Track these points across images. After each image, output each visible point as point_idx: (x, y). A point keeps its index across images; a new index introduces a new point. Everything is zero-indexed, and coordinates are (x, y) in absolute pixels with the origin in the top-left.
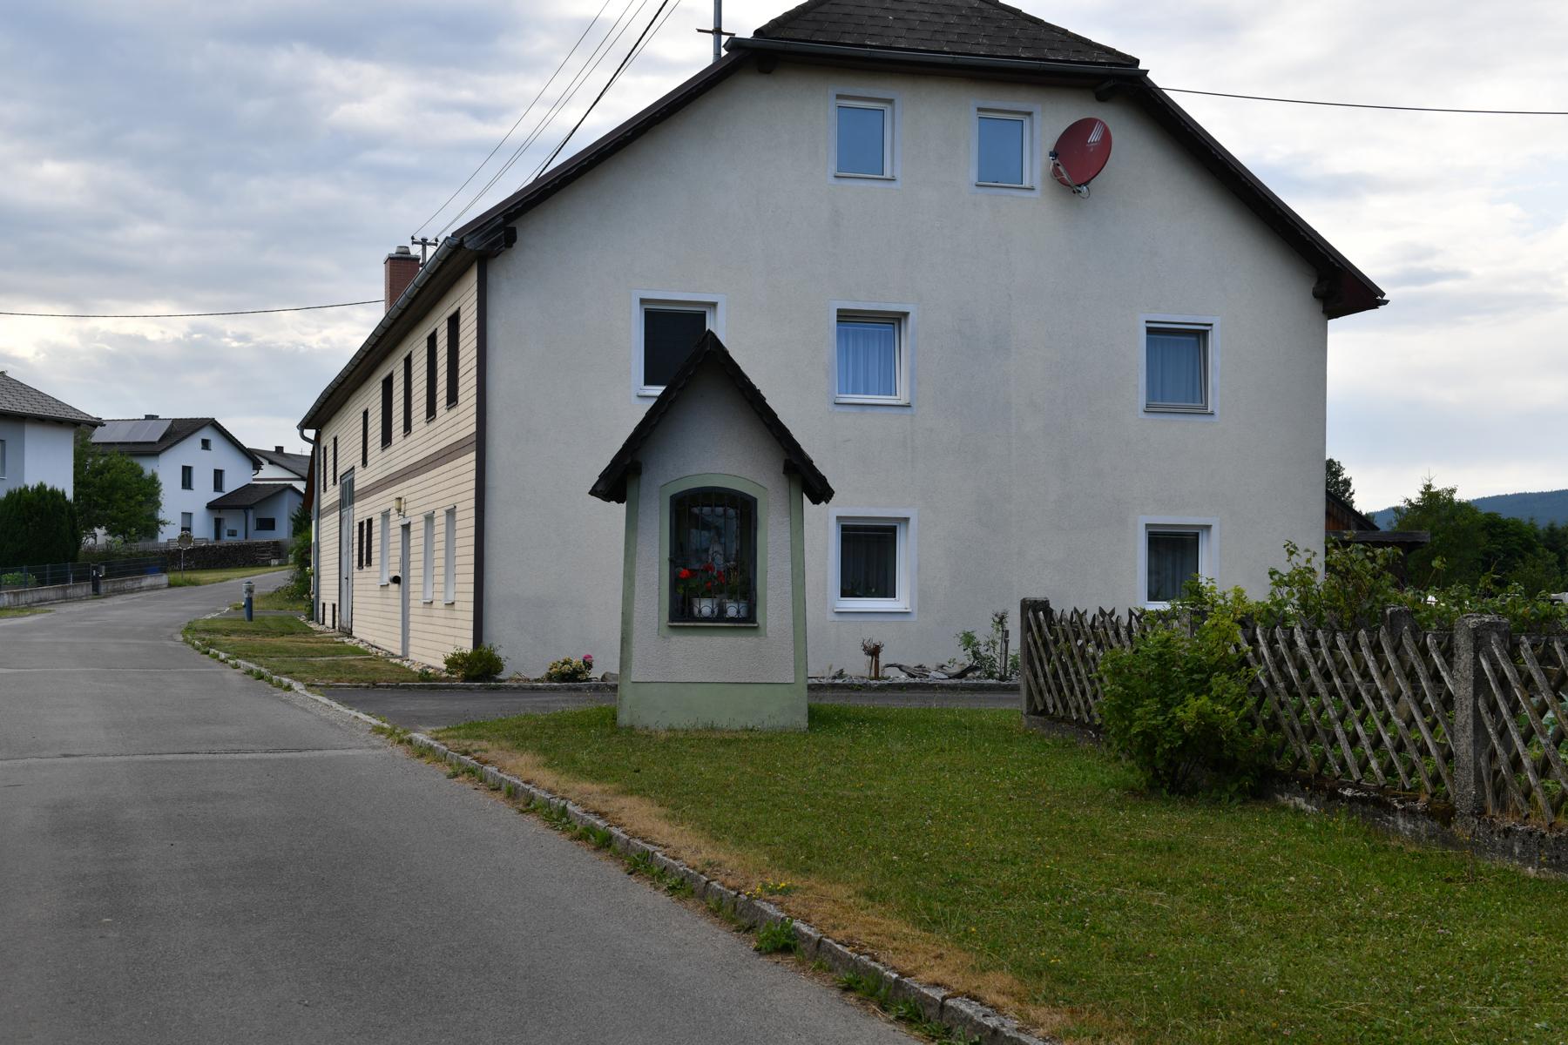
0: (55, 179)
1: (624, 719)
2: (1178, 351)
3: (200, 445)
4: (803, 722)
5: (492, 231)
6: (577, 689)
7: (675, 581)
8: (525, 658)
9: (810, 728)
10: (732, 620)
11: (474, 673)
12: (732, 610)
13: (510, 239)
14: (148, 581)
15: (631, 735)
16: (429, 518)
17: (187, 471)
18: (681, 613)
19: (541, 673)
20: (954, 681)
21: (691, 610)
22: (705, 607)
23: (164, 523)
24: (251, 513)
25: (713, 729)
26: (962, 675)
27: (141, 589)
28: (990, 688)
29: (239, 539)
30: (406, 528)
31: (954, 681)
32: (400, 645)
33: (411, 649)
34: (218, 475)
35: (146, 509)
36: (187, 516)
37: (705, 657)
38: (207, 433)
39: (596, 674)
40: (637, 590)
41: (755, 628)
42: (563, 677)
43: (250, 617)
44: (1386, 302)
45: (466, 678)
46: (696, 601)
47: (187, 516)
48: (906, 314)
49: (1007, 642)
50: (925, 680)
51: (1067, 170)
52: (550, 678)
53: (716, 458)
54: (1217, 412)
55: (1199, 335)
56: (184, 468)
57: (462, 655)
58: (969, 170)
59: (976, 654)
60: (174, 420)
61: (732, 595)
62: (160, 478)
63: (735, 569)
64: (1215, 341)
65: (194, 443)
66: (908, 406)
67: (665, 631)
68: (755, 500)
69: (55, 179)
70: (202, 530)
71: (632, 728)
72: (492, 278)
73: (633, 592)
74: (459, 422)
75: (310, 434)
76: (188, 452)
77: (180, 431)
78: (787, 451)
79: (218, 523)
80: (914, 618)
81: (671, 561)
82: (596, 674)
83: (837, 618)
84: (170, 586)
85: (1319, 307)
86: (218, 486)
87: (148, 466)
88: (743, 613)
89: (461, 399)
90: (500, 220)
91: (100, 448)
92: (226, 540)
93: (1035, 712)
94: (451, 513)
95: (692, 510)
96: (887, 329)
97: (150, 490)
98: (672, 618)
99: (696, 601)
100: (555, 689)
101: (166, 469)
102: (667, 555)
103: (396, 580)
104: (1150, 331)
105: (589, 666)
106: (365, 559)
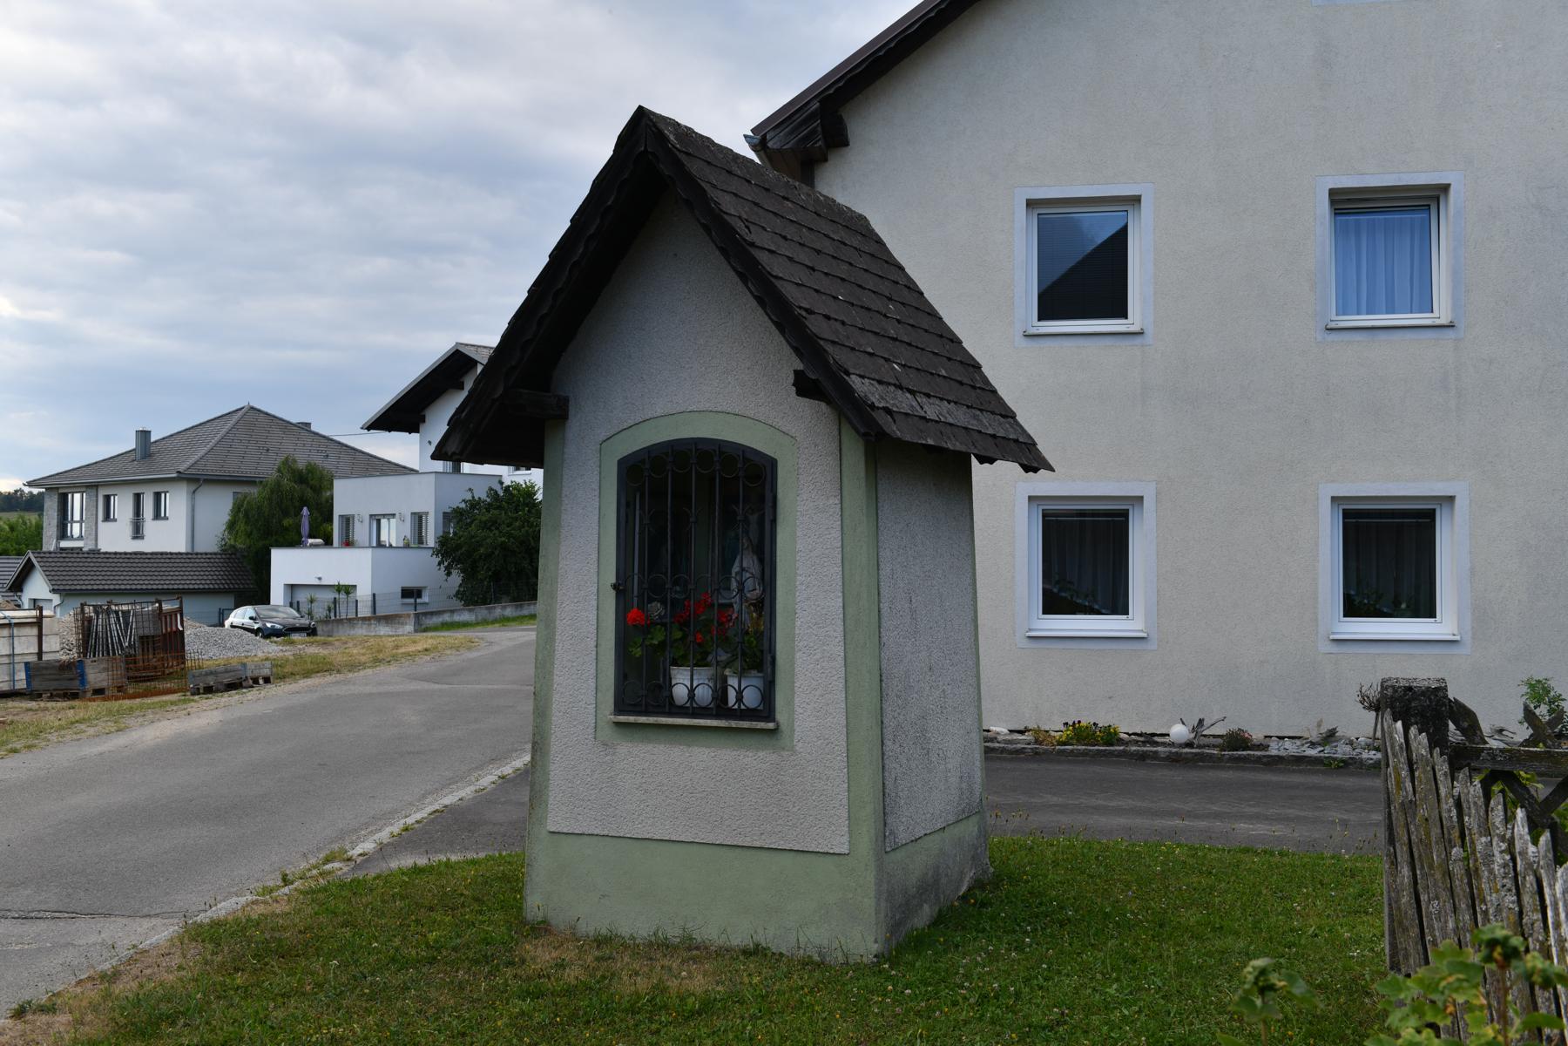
5: (805, 122)
37: (677, 785)
40: (559, 646)
41: (774, 732)
48: (1445, 188)
53: (699, 376)
66: (1451, 326)
68: (773, 463)
83: (1335, 649)
96: (1419, 216)
98: (621, 706)
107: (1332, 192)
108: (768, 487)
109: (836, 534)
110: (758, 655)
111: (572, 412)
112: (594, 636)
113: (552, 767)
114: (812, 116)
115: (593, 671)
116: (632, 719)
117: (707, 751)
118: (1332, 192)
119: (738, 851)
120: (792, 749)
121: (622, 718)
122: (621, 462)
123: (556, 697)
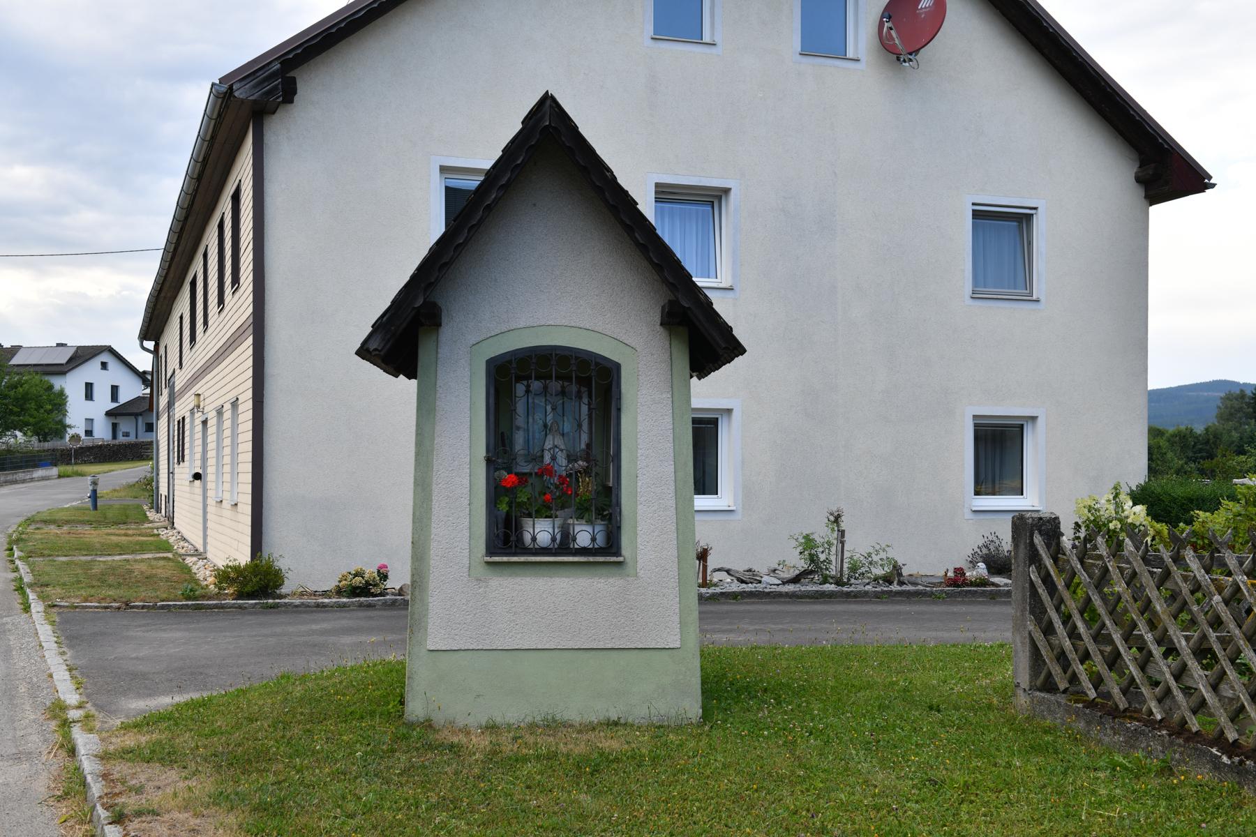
0: (22, 179)
1: (416, 708)
2: (1004, 231)
3: (99, 366)
4: (693, 708)
6: (370, 606)
7: (495, 492)
8: (308, 566)
9: (707, 714)
10: (583, 551)
11: (248, 589)
12: (584, 536)
13: (289, 94)
14: (39, 473)
15: (424, 738)
16: (220, 412)
17: (89, 387)
18: (505, 541)
19: (330, 585)
20: (790, 588)
21: (520, 539)
22: (542, 531)
23: (70, 427)
24: (140, 419)
25: (553, 726)
26: (795, 580)
27: (32, 480)
28: (830, 596)
29: (132, 439)
30: (205, 423)
31: (790, 588)
32: (201, 542)
33: (209, 547)
34: (115, 390)
35: (55, 416)
36: (90, 421)
37: (546, 606)
38: (105, 357)
39: (393, 583)
40: (436, 506)
42: (355, 591)
43: (95, 507)
44: (1213, 186)
45: (240, 595)
46: (527, 523)
47: (90, 421)
48: (727, 191)
49: (843, 543)
50: (760, 587)
51: (898, 32)
52: (339, 592)
53: (560, 297)
54: (1043, 299)
55: (1022, 220)
56: (87, 384)
57: (236, 569)
58: (794, 40)
59: (813, 559)
60: (79, 348)
61: (583, 512)
62: (67, 392)
63: (587, 471)
64: (1041, 228)
65: (95, 364)
67: (481, 570)
69: (22, 179)
70: (102, 432)
71: (428, 725)
72: (269, 138)
73: (429, 510)
74: (240, 305)
75: (150, 345)
76: (90, 371)
77: (82, 356)
78: (672, 286)
79: (115, 426)
80: (738, 516)
81: (489, 461)
82: (393, 583)
84: (60, 477)
85: (1139, 192)
86: (114, 397)
87: (58, 383)
88: (600, 541)
89: (242, 281)
90: (277, 66)
91: (16, 369)
92: (121, 439)
93: (1049, 686)
94: (235, 404)
95: (518, 377)
97: (58, 402)
98: (491, 551)
99: (527, 523)
100: (344, 605)
101: (72, 386)
102: (481, 452)
103: (197, 476)
104: (976, 215)
105: (384, 577)
106: (181, 458)
107: (657, 185)
108: (614, 383)
109: (669, 419)
110: (605, 505)
111: (444, 320)
112: (467, 496)
113: (431, 600)
114: (273, 76)
115: (467, 523)
116: (505, 559)
117: (566, 580)
118: (657, 185)
119: (593, 652)
120: (636, 575)
121: (488, 559)
122: (488, 362)
123: (433, 545)
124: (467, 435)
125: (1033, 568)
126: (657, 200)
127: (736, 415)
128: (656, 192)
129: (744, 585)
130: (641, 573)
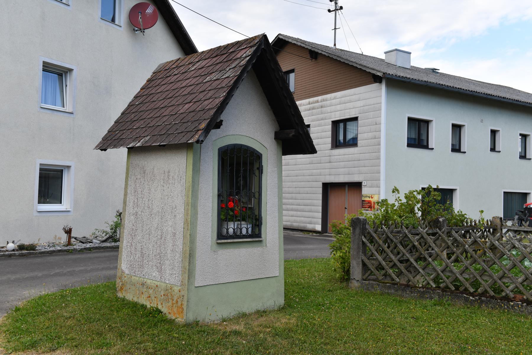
48: (71, 70)
58: (98, 13)
67: (215, 246)
73: (196, 219)
123: (198, 235)
124: (211, 183)
125: (363, 237)
126: (44, 70)
127: (72, 169)
128: (43, 66)
129: (85, 245)
130: (268, 245)
